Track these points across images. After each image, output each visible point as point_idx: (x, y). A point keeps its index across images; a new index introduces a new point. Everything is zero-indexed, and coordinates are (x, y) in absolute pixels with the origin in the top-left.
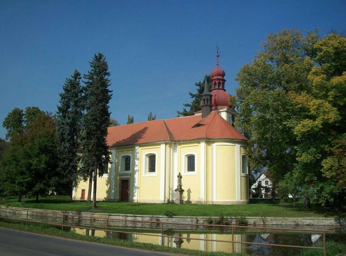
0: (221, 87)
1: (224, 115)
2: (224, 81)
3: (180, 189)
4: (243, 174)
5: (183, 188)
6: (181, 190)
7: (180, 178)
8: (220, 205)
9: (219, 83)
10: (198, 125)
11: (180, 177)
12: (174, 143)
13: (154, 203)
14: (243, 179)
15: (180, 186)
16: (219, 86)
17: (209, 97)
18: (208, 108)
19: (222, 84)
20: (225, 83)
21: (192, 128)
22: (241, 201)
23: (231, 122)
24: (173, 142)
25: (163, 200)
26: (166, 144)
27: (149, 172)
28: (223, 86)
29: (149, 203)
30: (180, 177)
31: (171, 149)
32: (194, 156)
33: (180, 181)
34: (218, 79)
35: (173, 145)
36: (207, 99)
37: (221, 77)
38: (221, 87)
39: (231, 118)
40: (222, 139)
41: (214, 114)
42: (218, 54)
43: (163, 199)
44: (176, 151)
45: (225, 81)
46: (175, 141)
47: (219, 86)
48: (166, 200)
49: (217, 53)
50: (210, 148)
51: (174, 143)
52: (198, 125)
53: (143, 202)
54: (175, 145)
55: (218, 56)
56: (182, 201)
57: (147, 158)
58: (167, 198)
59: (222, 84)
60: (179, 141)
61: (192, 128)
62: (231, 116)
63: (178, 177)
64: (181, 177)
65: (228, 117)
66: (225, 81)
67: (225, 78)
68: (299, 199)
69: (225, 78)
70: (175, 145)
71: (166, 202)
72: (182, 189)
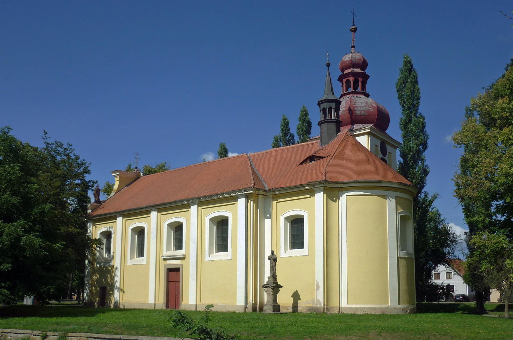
0: (359, 89)
1: (364, 141)
2: (366, 77)
4: (402, 254)
5: (280, 281)
6: (274, 285)
7: (273, 261)
9: (356, 82)
10: (312, 158)
11: (273, 259)
13: (133, 308)
14: (403, 262)
15: (274, 277)
16: (355, 88)
17: (333, 105)
18: (333, 126)
19: (360, 83)
20: (368, 82)
21: (300, 164)
22: (399, 306)
23: (380, 156)
24: (261, 192)
26: (248, 197)
28: (364, 87)
29: (188, 310)
30: (273, 259)
33: (273, 268)
34: (353, 74)
35: (261, 198)
36: (330, 108)
37: (358, 70)
38: (359, 89)
39: (379, 148)
40: (354, 182)
42: (354, 27)
43: (243, 303)
45: (368, 77)
46: (264, 190)
47: (355, 88)
48: (250, 305)
50: (333, 205)
52: (312, 158)
53: (132, 308)
54: (265, 198)
55: (355, 30)
56: (277, 308)
59: (360, 83)
60: (273, 190)
61: (300, 164)
62: (378, 143)
64: (275, 260)
65: (371, 143)
66: (368, 77)
70: (265, 198)
71: (249, 310)
72: (277, 283)
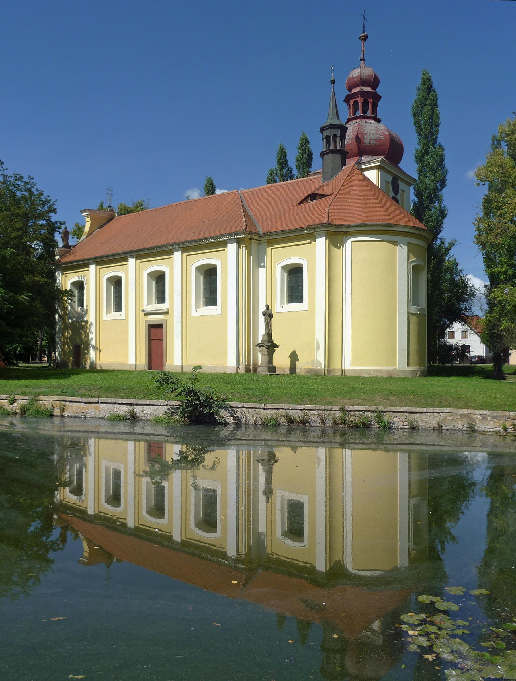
0: (369, 113)
2: (377, 98)
3: (269, 342)
5: (276, 339)
6: (270, 344)
7: (268, 317)
8: (195, 518)
9: (365, 104)
10: (313, 196)
11: (269, 315)
12: (258, 238)
14: (414, 319)
15: (269, 335)
17: (338, 132)
18: (337, 158)
19: (370, 106)
20: (380, 103)
22: (408, 369)
23: (392, 194)
25: (234, 367)
26: (239, 242)
27: (206, 306)
28: (374, 111)
31: (246, 250)
32: (303, 268)
33: (268, 325)
34: (362, 93)
36: (335, 136)
38: (369, 113)
39: (390, 185)
41: (350, 171)
42: (364, 34)
44: (263, 264)
45: (378, 98)
46: (257, 234)
49: (362, 29)
51: (258, 238)
52: (313, 196)
54: (259, 244)
57: (201, 277)
58: (244, 363)
59: (370, 106)
60: (268, 234)
61: (299, 204)
62: (390, 178)
63: (264, 315)
64: (271, 316)
65: (382, 179)
66: (378, 98)
67: (379, 91)
68: (92, 365)
69: (379, 91)
70: (259, 244)
